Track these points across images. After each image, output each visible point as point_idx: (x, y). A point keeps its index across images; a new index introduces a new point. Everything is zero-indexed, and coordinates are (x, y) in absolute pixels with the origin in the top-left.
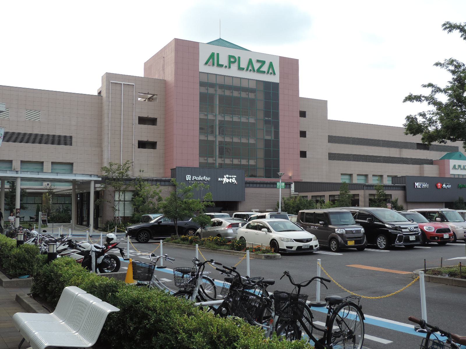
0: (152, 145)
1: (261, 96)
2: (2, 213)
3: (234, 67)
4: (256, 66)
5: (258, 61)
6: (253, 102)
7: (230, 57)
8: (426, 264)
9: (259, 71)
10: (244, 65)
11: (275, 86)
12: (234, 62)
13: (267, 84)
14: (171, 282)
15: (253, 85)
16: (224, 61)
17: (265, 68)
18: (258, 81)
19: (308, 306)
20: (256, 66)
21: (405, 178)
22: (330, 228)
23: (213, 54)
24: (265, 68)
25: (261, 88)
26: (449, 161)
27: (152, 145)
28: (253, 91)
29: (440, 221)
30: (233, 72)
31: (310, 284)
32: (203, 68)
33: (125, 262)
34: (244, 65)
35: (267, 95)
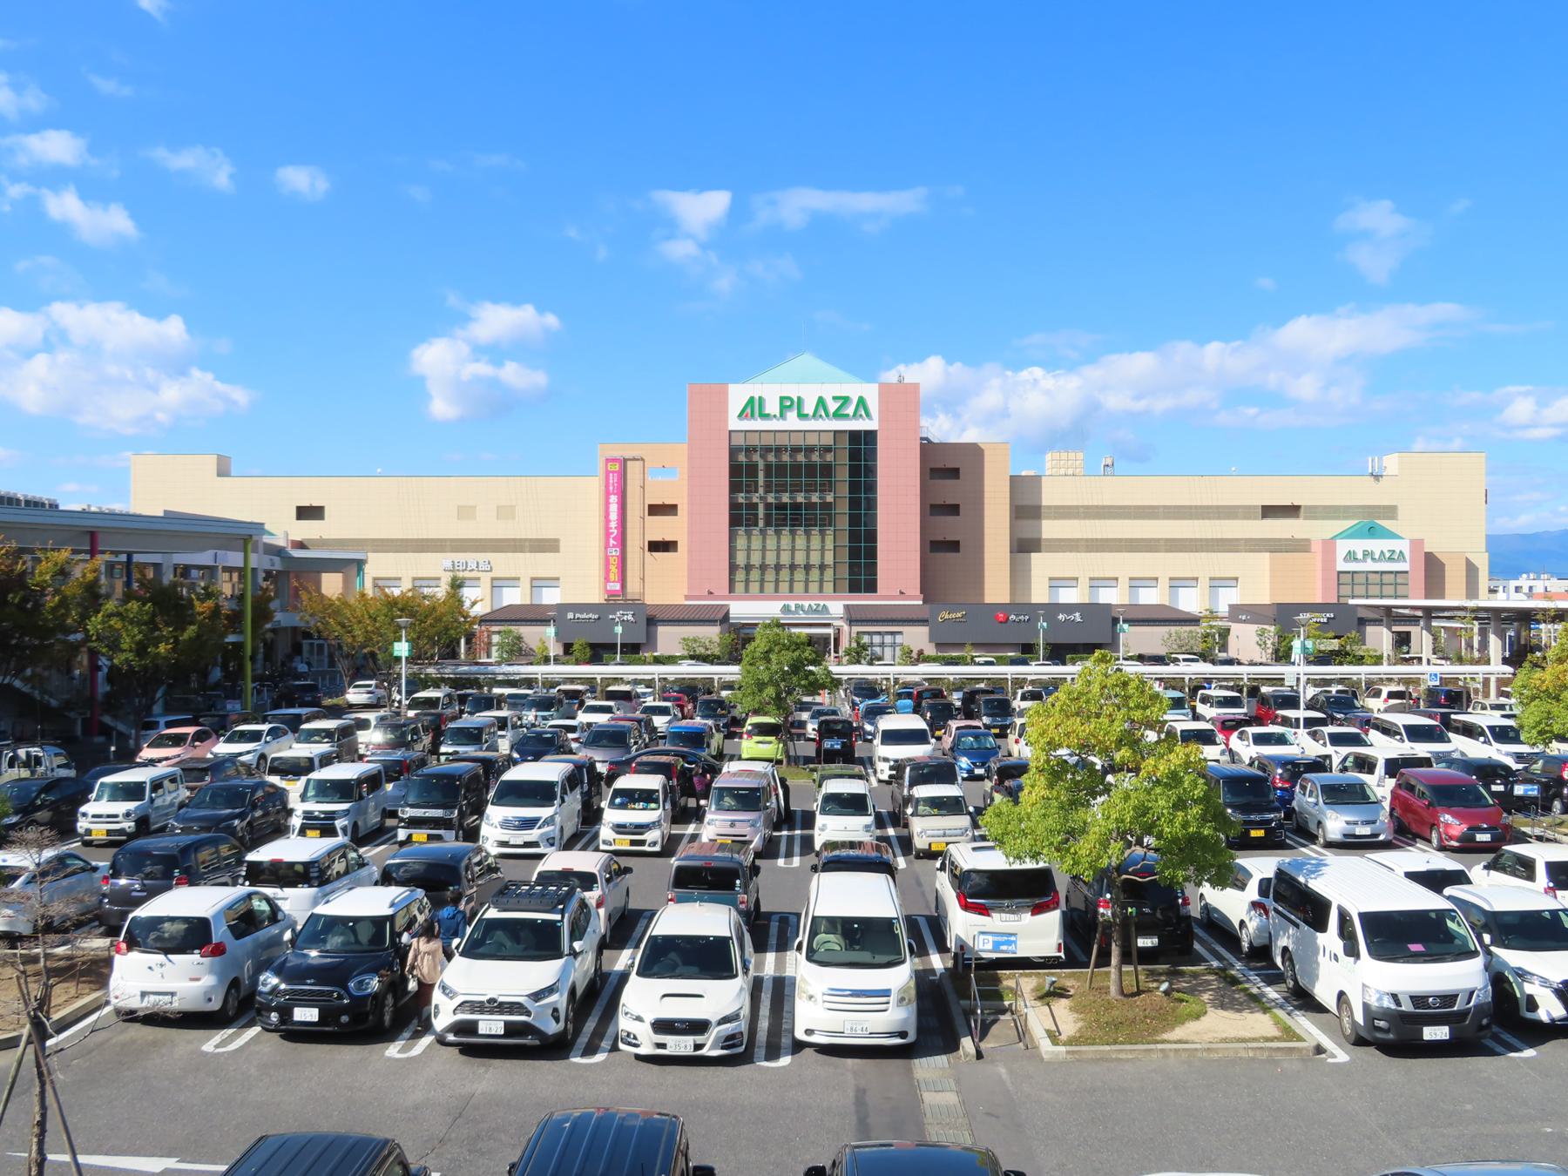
0: (655, 510)
1: (844, 459)
3: (792, 415)
4: (833, 406)
7: (782, 399)
9: (838, 415)
10: (809, 408)
11: (870, 436)
13: (855, 436)
15: (828, 440)
16: (772, 407)
17: (850, 410)
19: (643, 946)
20: (833, 406)
21: (1133, 622)
23: (752, 399)
24: (850, 410)
25: (845, 443)
27: (655, 510)
29: (216, 1005)
30: (792, 422)
32: (735, 424)
33: (880, 412)
34: (809, 408)
35: (854, 455)
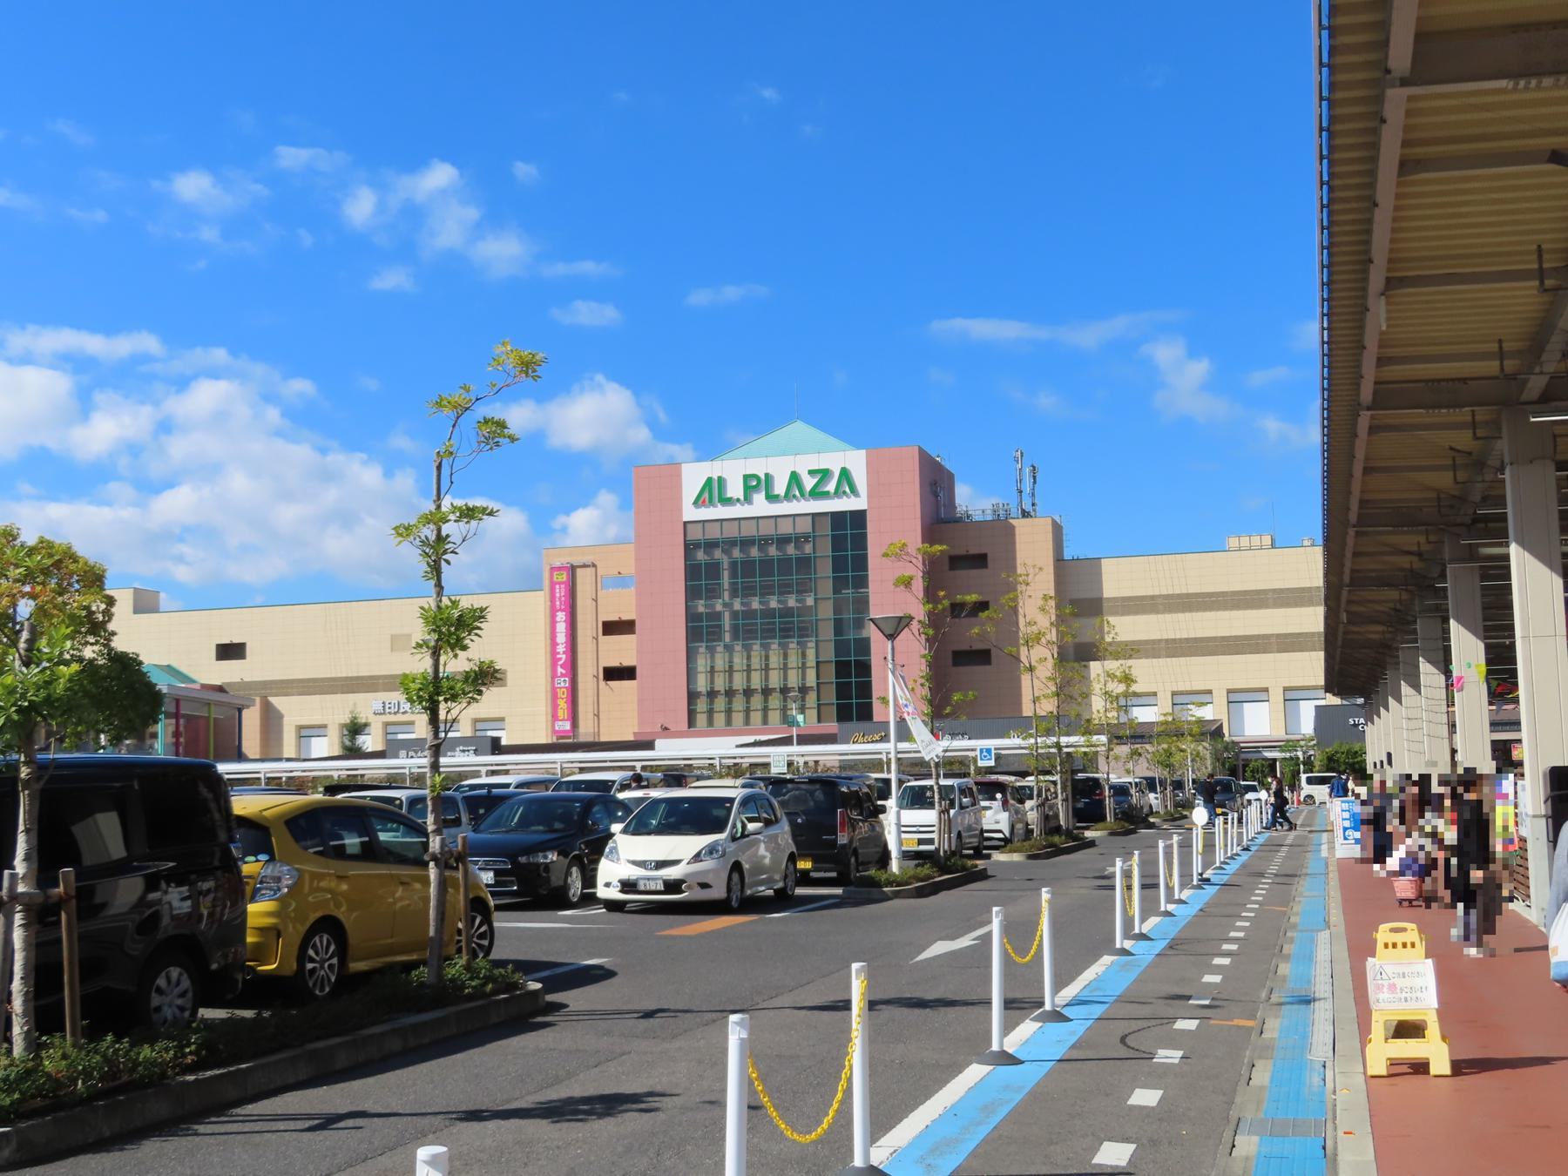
1: (825, 548)
2: (1444, 1038)
3: (759, 498)
4: (809, 483)
5: (811, 473)
6: (805, 563)
7: (746, 478)
8: (326, 755)
10: (780, 488)
11: (859, 518)
12: (756, 489)
13: (838, 518)
14: (919, 953)
15: (805, 527)
16: (735, 489)
18: (814, 515)
20: (809, 483)
22: (1210, 984)
23: (709, 480)
25: (826, 529)
26: (1318, 604)
28: (800, 540)
30: (760, 506)
31: (917, 1011)
32: (690, 513)
34: (780, 488)
35: (838, 544)
